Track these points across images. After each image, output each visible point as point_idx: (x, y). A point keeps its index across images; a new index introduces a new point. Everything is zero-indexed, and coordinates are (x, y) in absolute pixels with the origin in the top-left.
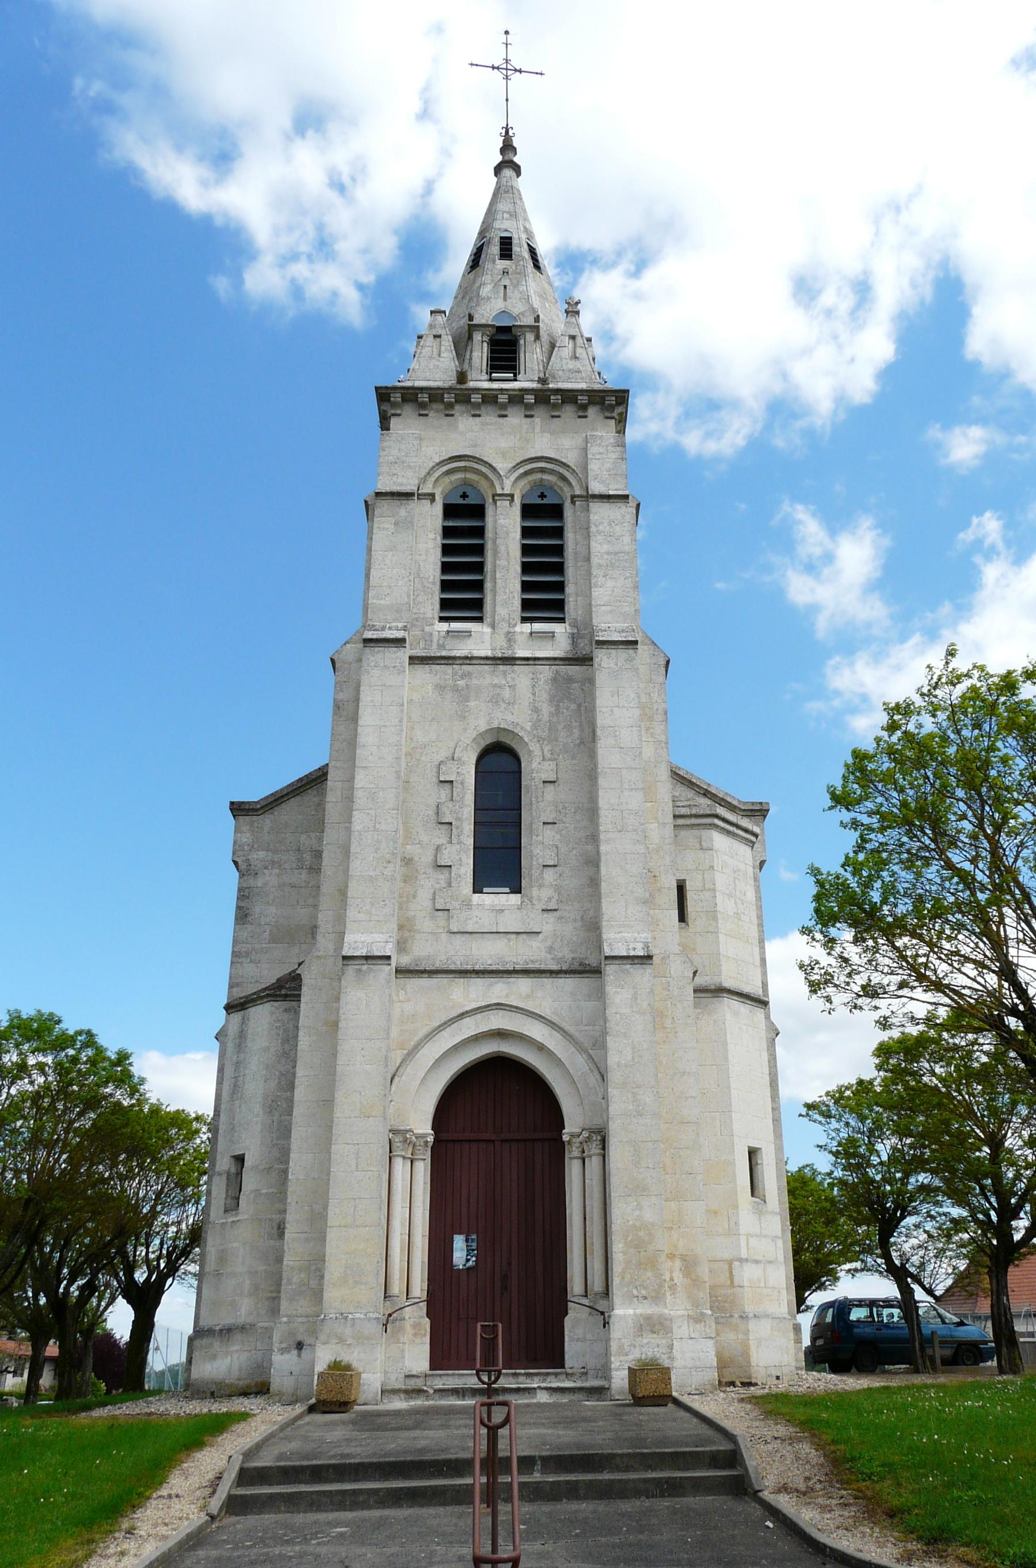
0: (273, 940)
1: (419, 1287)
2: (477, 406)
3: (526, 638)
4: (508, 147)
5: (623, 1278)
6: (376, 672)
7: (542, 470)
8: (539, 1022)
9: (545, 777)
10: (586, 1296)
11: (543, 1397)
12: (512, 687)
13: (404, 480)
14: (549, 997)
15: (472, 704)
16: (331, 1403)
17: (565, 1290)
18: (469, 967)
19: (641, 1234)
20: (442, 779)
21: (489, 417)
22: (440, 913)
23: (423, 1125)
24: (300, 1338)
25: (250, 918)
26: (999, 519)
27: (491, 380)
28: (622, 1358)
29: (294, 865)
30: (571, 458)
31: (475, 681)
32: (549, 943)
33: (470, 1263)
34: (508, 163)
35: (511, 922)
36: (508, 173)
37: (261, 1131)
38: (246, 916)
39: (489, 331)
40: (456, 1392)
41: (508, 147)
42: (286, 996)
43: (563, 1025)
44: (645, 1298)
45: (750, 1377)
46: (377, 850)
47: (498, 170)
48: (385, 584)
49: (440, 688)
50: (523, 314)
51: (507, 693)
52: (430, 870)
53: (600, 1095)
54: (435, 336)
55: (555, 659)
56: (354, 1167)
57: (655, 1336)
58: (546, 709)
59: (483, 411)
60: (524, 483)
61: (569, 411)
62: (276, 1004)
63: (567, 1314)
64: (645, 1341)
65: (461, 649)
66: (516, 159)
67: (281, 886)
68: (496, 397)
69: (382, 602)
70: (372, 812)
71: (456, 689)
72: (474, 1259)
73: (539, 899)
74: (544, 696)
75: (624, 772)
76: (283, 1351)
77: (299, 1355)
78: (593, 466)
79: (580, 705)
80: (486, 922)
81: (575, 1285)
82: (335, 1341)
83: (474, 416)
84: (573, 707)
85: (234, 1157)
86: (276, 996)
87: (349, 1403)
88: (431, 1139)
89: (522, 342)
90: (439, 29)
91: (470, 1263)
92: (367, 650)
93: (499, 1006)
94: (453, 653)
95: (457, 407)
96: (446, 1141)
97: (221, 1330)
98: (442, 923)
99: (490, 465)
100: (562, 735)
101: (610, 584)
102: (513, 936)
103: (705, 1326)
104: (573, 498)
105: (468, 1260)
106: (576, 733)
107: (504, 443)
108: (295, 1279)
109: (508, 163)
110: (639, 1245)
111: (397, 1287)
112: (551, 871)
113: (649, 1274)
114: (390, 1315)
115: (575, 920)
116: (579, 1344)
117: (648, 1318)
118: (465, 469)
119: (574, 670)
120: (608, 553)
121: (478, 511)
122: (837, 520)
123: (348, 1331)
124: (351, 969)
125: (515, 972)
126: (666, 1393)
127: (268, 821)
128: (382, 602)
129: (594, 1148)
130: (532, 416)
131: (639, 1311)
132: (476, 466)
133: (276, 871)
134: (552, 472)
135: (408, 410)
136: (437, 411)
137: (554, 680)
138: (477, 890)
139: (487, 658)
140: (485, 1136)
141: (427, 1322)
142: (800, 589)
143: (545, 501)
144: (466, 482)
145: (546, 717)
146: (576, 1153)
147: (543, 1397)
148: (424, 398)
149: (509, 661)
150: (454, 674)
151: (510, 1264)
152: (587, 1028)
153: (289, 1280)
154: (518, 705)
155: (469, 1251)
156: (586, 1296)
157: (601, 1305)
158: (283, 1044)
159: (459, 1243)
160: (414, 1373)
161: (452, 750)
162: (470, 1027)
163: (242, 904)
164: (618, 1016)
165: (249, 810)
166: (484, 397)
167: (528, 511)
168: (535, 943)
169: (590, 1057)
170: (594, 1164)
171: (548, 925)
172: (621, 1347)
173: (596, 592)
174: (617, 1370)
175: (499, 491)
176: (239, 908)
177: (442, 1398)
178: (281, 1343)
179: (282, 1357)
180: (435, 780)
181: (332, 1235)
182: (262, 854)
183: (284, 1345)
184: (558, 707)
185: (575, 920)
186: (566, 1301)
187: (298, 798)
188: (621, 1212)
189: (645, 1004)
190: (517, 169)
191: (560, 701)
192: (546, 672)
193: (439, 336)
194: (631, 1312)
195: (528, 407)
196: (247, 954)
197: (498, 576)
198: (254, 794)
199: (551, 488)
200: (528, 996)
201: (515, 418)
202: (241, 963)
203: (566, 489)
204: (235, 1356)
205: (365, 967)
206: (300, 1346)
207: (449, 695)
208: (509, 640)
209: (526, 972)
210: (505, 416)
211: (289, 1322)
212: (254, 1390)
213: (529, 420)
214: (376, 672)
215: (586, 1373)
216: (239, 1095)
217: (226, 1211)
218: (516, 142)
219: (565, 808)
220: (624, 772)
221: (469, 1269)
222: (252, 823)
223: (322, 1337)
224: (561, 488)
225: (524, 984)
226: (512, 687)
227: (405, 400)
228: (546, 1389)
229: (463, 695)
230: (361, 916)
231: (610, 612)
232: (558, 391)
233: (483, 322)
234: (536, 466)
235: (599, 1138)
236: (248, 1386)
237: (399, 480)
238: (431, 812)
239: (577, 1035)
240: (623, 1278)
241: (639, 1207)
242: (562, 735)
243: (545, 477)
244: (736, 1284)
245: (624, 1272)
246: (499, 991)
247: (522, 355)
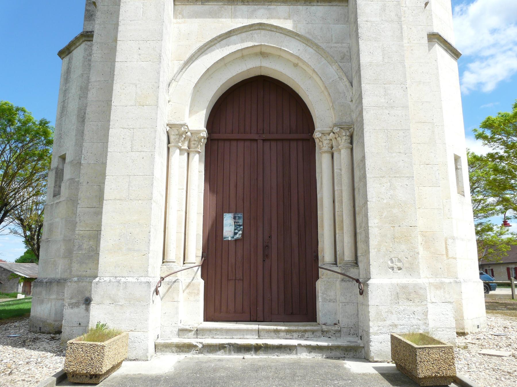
1: (195, 253)
5: (379, 251)
10: (336, 264)
16: (81, 375)
17: (316, 258)
23: (198, 123)
28: (380, 323)
37: (76, 135)
38: (92, 15)
44: (400, 269)
45: (463, 329)
53: (349, 99)
57: (411, 303)
63: (318, 278)
64: (402, 308)
72: (240, 232)
76: (73, 305)
81: (326, 254)
82: (108, 302)
87: (100, 375)
88: (205, 134)
91: (237, 236)
96: (218, 140)
97: (46, 282)
103: (445, 292)
105: (235, 234)
108: (85, 246)
111: (174, 253)
114: (163, 279)
116: (331, 304)
117: (404, 287)
126: (449, 373)
129: (343, 142)
141: (201, 283)
151: (270, 237)
152: (336, 45)
155: (237, 226)
156: (336, 264)
157: (353, 272)
160: (188, 327)
163: (89, 8)
164: (369, 24)
170: (343, 157)
174: (376, 334)
176: (87, 10)
178: (71, 298)
179: (72, 311)
181: (107, 207)
183: (74, 301)
186: (317, 268)
188: (376, 191)
215: (340, 331)
216: (65, 113)
221: (236, 240)
235: (348, 134)
240: (379, 251)
244: (450, 256)
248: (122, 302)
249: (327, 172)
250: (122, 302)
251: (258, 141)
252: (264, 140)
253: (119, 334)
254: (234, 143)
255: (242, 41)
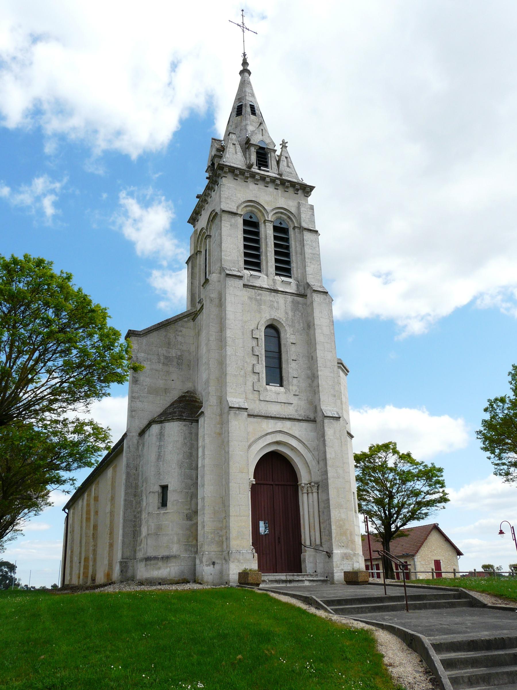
0: (149, 393)
2: (257, 180)
3: (279, 282)
4: (245, 63)
6: (231, 288)
7: (282, 213)
8: (295, 439)
9: (292, 341)
11: (307, 583)
12: (277, 302)
13: (231, 207)
14: (299, 430)
15: (263, 307)
18: (269, 415)
19: (341, 523)
20: (254, 337)
21: (261, 186)
22: (255, 392)
24: (214, 560)
25: (138, 382)
26: (34, 179)
27: (260, 169)
29: (157, 361)
30: (293, 210)
31: (263, 298)
32: (296, 408)
33: (266, 532)
34: (245, 71)
35: (282, 398)
36: (246, 74)
39: (257, 148)
40: (277, 581)
41: (245, 63)
42: (185, 419)
43: (303, 441)
46: (237, 364)
47: (241, 73)
48: (228, 250)
49: (250, 298)
50: (270, 143)
51: (275, 304)
52: (251, 374)
54: (233, 144)
55: (293, 293)
56: (238, 492)
58: (290, 314)
59: (270, 185)
60: (275, 216)
61: (291, 190)
62: (181, 422)
65: (257, 283)
66: (249, 68)
67: (151, 369)
68: (265, 178)
69: (227, 258)
70: (234, 347)
71: (256, 300)
73: (292, 390)
74: (289, 308)
75: (325, 344)
77: (214, 567)
78: (303, 216)
79: (302, 314)
80: (273, 398)
83: (255, 184)
84: (300, 314)
85: (160, 486)
86: (181, 419)
89: (269, 155)
90: (243, 10)
91: (266, 532)
92: (227, 279)
93: (280, 432)
94: (255, 285)
95: (240, 176)
98: (257, 396)
99: (263, 207)
100: (297, 325)
101: (312, 266)
102: (283, 404)
104: (294, 228)
106: (302, 325)
107: (268, 198)
108: (209, 537)
109: (245, 71)
110: (340, 527)
112: (295, 379)
113: (344, 538)
115: (305, 400)
117: (345, 554)
118: (252, 206)
119: (299, 299)
120: (311, 253)
121: (256, 225)
122: (146, 204)
123: (241, 557)
124: (232, 412)
125: (286, 418)
127: (145, 340)
128: (227, 258)
130: (277, 189)
131: (342, 551)
132: (257, 206)
133: (149, 363)
134: (285, 214)
135: (230, 176)
136: (241, 179)
137: (293, 302)
138: (267, 384)
139: (268, 289)
140: (267, 483)
142: (129, 232)
143: (282, 226)
144: (251, 212)
145: (290, 317)
146: (305, 491)
147: (307, 583)
148: (237, 172)
149: (276, 291)
150: (256, 293)
153: (207, 537)
154: (280, 309)
158: (184, 439)
159: (262, 524)
161: (256, 325)
162: (270, 439)
165: (137, 334)
166: (271, 179)
167: (276, 229)
168: (291, 407)
169: (313, 455)
171: (294, 400)
172: (337, 565)
173: (308, 269)
174: (336, 573)
175: (267, 219)
177: (272, 583)
180: (251, 336)
182: (143, 355)
183: (208, 563)
184: (294, 313)
185: (305, 400)
187: (157, 332)
189: (338, 435)
190: (249, 73)
191: (295, 311)
192: (289, 298)
193: (235, 144)
194: (339, 552)
195: (277, 185)
196: (138, 398)
197: (268, 254)
198: (140, 327)
199: (284, 221)
200: (290, 428)
201: (271, 189)
202: (136, 402)
203: (290, 223)
204: (172, 568)
205: (237, 412)
206: (214, 563)
207: (254, 302)
208: (274, 282)
209: (290, 419)
210: (268, 187)
211: (208, 554)
212: (181, 582)
213: (276, 190)
214: (231, 288)
217: (158, 508)
218: (248, 61)
219: (299, 355)
220: (325, 344)
221: (266, 535)
222: (138, 340)
223: (232, 559)
224: (288, 222)
225: (288, 424)
226: (277, 302)
227: (230, 171)
228: (308, 580)
229: (259, 303)
230: (232, 391)
231: (313, 278)
232: (289, 181)
233: (254, 143)
234: (281, 211)
236: (179, 580)
237: (230, 206)
238: (250, 350)
239: (308, 445)
241: (340, 513)
242: (297, 325)
243: (282, 216)
245: (336, 537)
246: (279, 425)
247: (270, 161)
248: (242, 561)
249: (307, 504)
250: (242, 561)
251: (274, 486)
252: (276, 485)
253: (200, 584)
254: (262, 486)
255: (485, 653)
